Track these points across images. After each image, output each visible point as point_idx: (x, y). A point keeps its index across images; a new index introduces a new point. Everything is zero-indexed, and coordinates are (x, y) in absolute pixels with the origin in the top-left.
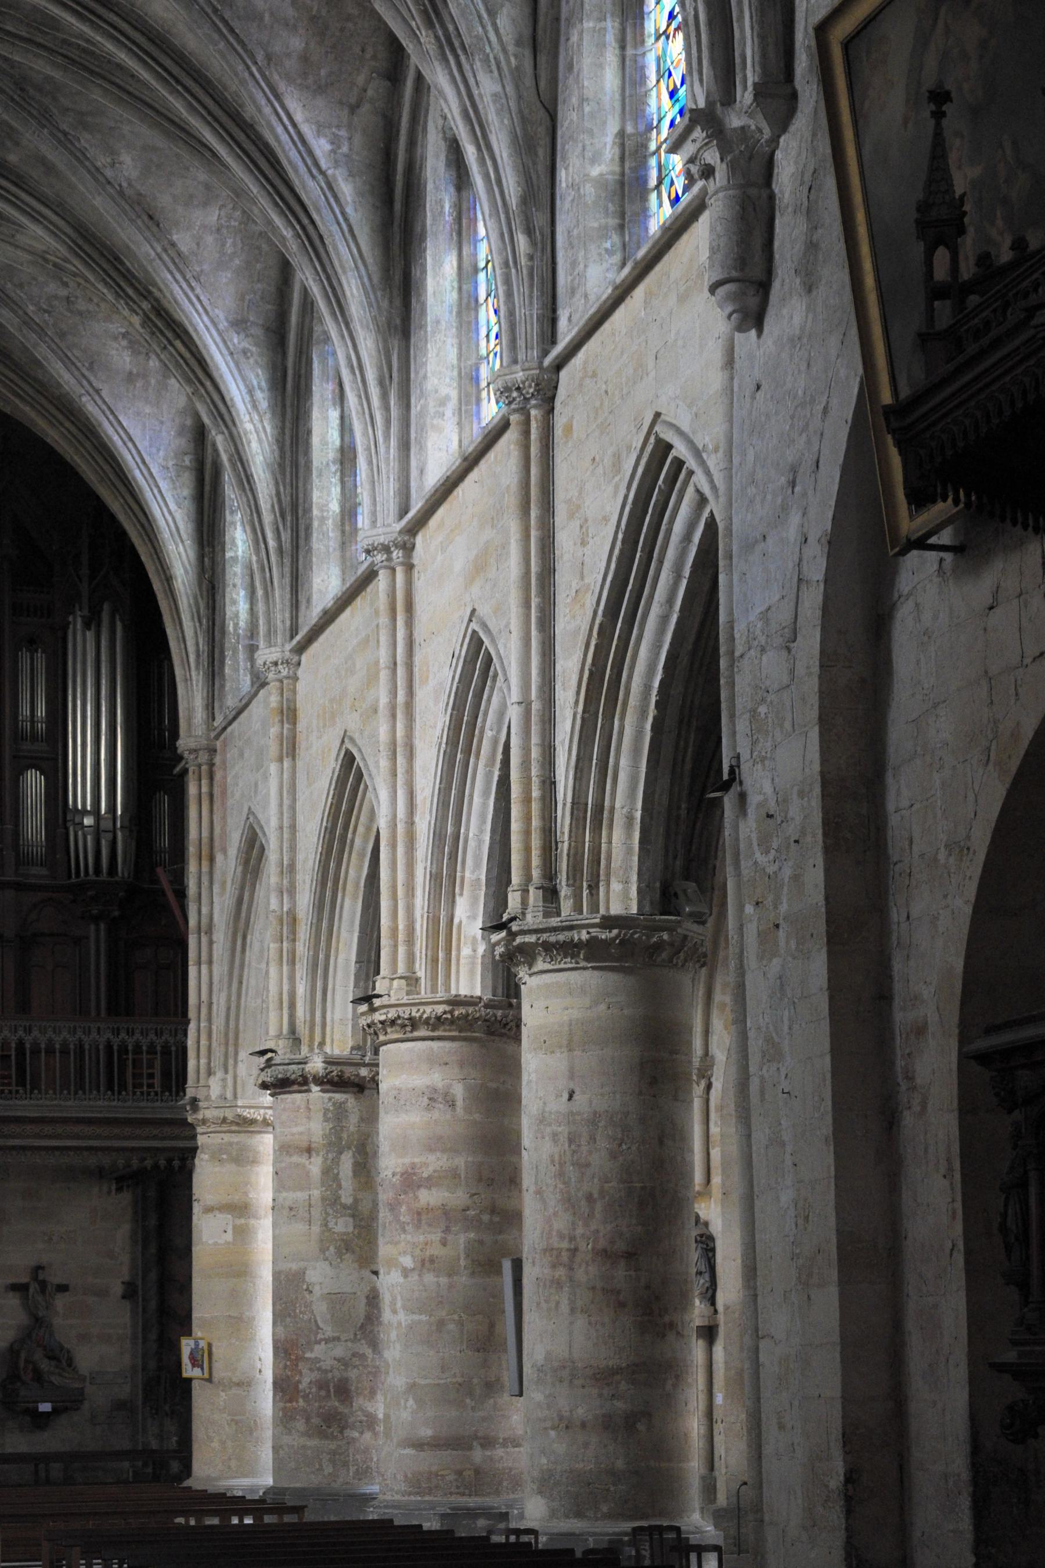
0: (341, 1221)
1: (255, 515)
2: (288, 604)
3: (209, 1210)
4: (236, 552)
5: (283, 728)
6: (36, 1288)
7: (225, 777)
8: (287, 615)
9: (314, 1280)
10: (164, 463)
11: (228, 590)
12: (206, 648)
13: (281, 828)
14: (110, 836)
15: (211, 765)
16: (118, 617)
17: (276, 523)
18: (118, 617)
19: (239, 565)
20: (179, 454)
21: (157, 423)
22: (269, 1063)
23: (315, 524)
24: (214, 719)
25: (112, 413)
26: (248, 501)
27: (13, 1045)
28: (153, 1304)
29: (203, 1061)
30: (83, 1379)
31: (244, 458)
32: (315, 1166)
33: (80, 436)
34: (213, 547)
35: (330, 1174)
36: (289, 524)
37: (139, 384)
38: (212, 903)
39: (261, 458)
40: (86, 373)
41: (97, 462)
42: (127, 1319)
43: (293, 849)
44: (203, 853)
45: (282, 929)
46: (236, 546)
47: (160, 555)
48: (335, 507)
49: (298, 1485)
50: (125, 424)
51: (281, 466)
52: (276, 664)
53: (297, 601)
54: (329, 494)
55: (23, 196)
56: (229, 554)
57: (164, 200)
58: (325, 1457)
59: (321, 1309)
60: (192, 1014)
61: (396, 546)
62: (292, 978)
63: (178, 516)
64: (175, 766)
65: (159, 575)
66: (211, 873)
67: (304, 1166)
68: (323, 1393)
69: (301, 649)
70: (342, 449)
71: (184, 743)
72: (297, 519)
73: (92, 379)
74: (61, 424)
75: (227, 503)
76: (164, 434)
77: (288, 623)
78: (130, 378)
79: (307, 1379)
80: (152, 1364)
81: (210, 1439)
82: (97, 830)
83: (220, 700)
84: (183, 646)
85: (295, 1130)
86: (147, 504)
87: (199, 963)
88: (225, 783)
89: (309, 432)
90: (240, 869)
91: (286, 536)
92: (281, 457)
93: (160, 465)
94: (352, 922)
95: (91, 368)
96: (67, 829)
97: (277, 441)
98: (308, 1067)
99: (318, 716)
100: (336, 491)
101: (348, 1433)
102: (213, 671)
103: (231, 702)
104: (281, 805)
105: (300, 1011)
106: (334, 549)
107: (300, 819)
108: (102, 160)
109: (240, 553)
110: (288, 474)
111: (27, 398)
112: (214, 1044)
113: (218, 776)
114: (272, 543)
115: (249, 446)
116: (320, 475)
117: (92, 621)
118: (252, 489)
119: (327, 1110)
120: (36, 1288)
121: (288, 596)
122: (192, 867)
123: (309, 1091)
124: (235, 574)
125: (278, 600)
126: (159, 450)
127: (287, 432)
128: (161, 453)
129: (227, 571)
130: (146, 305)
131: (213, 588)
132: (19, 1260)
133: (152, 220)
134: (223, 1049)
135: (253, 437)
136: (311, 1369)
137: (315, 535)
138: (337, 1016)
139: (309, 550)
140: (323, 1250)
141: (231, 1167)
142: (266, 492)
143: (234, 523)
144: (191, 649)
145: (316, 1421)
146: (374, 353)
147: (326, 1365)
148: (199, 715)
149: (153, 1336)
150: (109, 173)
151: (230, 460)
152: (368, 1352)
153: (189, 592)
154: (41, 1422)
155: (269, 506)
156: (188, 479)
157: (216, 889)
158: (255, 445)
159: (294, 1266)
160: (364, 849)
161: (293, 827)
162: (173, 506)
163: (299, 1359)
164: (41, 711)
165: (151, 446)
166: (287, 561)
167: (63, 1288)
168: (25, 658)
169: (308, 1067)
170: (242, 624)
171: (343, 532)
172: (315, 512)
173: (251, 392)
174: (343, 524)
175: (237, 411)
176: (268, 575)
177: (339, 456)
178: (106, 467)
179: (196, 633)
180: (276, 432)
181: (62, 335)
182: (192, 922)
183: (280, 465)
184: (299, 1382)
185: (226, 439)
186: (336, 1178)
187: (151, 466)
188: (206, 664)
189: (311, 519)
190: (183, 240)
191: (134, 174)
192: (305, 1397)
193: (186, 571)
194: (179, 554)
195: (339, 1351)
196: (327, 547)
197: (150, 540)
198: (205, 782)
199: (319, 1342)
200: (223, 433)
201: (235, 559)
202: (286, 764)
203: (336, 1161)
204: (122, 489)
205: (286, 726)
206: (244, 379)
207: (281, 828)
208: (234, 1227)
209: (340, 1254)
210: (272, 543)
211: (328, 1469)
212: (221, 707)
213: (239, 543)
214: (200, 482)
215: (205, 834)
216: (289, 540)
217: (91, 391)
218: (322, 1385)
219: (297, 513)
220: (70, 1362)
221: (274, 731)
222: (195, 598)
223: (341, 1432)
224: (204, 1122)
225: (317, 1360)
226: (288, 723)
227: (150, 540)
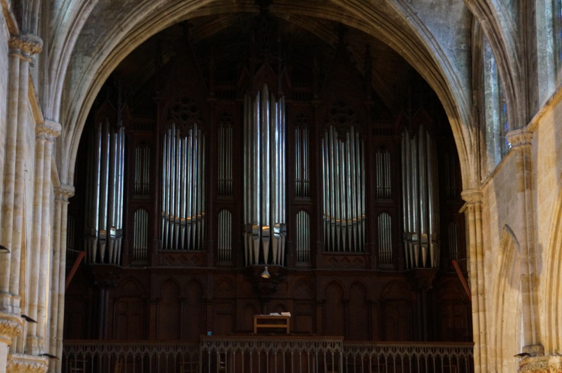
1: (504, 61)
2: (524, 105)
4: (491, 90)
5: (524, 173)
7: (488, 209)
8: (524, 112)
10: (450, 48)
11: (487, 110)
12: (475, 142)
14: (426, 245)
16: (427, 133)
17: (516, 63)
18: (427, 133)
19: (492, 97)
20: (459, 43)
21: (446, 28)
23: (539, 60)
24: (481, 179)
25: (423, 25)
26: (500, 53)
27: (378, 358)
29: (483, 366)
31: (497, 31)
33: (407, 40)
34: (478, 90)
36: (523, 63)
37: (437, 9)
38: (484, 278)
39: (507, 30)
40: (409, 5)
41: (414, 51)
44: (478, 251)
45: (529, 284)
46: (491, 88)
47: (449, 96)
50: (429, 29)
51: (518, 33)
53: (529, 104)
54: (546, 43)
56: (486, 92)
60: (475, 339)
64: (460, 208)
65: (449, 107)
66: (483, 262)
72: (528, 60)
73: (412, 8)
74: (397, 34)
75: (485, 66)
76: (450, 34)
77: (525, 116)
82: (419, 241)
83: (484, 168)
84: (463, 142)
86: (442, 70)
87: (478, 311)
88: (489, 213)
89: (534, 13)
91: (522, 70)
92: (518, 28)
93: (448, 49)
95: (411, 3)
96: (403, 243)
97: (515, 20)
99: (545, 163)
102: (480, 154)
106: (551, 73)
109: (493, 90)
110: (522, 37)
111: (379, 22)
112: (489, 357)
113: (484, 210)
114: (514, 74)
115: (500, 24)
116: (541, 34)
117: (414, 134)
118: (501, 47)
121: (524, 102)
122: (472, 259)
124: (490, 102)
125: (518, 104)
126: (447, 42)
127: (521, 15)
128: (449, 44)
129: (486, 101)
131: (478, 111)
134: (494, 359)
137: (539, 66)
139: (536, 75)
142: (510, 47)
143: (489, 76)
144: (467, 143)
148: (473, 177)
151: (489, 33)
153: (465, 114)
155: (512, 55)
156: (463, 57)
158: (503, 23)
162: (455, 70)
164: (388, 184)
165: (443, 40)
166: (523, 83)
168: (379, 155)
170: (495, 127)
171: (556, 63)
172: (539, 54)
174: (555, 59)
175: (493, 6)
176: (512, 91)
177: (552, 23)
178: (420, 54)
179: (470, 135)
180: (514, 15)
182: (473, 289)
183: (517, 33)
185: (486, 22)
187: (444, 50)
188: (476, 151)
189: (536, 58)
193: (463, 102)
194: (460, 94)
196: (546, 72)
197: (444, 89)
198: (477, 213)
200: (485, 19)
201: (490, 94)
204: (429, 64)
205: (526, 172)
210: (514, 74)
212: (485, 172)
213: (492, 86)
214: (470, 57)
215: (479, 240)
216: (523, 72)
217: (412, 14)
219: (527, 57)
221: (519, 175)
222: (469, 116)
226: (527, 169)
227: (444, 89)
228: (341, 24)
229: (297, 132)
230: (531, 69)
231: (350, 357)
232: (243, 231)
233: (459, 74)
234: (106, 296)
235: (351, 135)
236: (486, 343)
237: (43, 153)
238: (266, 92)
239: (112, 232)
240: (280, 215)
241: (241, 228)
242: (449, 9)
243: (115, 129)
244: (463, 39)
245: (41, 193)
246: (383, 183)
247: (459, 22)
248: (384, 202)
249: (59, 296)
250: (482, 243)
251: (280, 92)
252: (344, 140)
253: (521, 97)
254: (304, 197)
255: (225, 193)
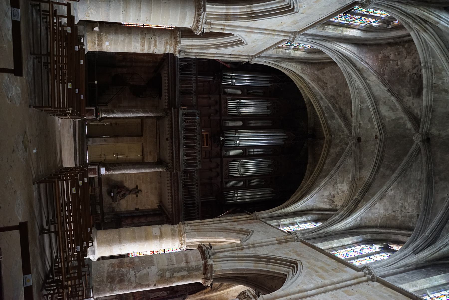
0: (169, 274)
3: (160, 229)
6: (137, 191)
9: (152, 268)
13: (262, 243)
15: (253, 219)
22: (208, 248)
28: (135, 214)
30: (119, 201)
32: (183, 265)
35: (181, 269)
42: (132, 209)
43: (259, 246)
48: (334, 246)
49: (93, 271)
51: (336, 232)
52: (297, 236)
55: (375, 172)
57: (385, 200)
58: (101, 278)
59: (144, 271)
60: (203, 221)
61: (372, 276)
62: (228, 251)
63: (299, 207)
67: (182, 262)
68: (120, 275)
69: (301, 241)
70: (345, 245)
71: (257, 213)
78: (323, 196)
79: (124, 270)
80: (122, 215)
81: (106, 235)
85: (192, 257)
90: (238, 229)
91: (323, 235)
94: (247, 266)
98: (209, 260)
100: (337, 245)
101: (109, 284)
103: (268, 222)
104: (267, 242)
105: (221, 255)
107: (265, 247)
108: (392, 187)
113: (251, 221)
116: (340, 241)
119: (198, 266)
120: (137, 191)
123: (202, 260)
130: (360, 198)
132: (143, 187)
133: (381, 198)
135: (341, 225)
136: (127, 271)
138: (222, 265)
140: (161, 270)
141: (171, 234)
145: (112, 274)
146: (411, 262)
147: (129, 276)
148: (263, 216)
149: (128, 215)
150: (390, 189)
151: (334, 220)
152: (133, 286)
154: (109, 194)
157: (229, 223)
159: (155, 262)
160: (268, 268)
161: (263, 246)
163: (130, 267)
166: (318, 236)
167: (137, 196)
169: (209, 260)
173: (350, 223)
181: (330, 182)
182: (221, 219)
184: (123, 268)
186: (180, 271)
190: (377, 205)
191: (389, 194)
192: (119, 270)
195: (133, 279)
199: (135, 272)
201: (294, 220)
202: (277, 242)
203: (185, 270)
206: (352, 221)
207: (262, 243)
208: (157, 236)
209: (160, 275)
210: (321, 231)
211: (98, 280)
215: (240, 219)
218: (123, 275)
220: (122, 199)
223: (109, 282)
224: (180, 226)
225: (130, 273)
228: (307, 164)
229: (271, 150)
230: (324, 238)
231: (193, 172)
232: (236, 130)
233: (299, 207)
234: (210, 78)
235: (270, 169)
236: (202, 225)
237: (286, 34)
238: (286, 137)
239: (234, 80)
240: (243, 144)
241: (237, 129)
242: (321, 202)
243: (270, 82)
244: (310, 208)
245: (270, 33)
246: (253, 182)
247: (316, 206)
248: (246, 182)
249: (214, 56)
250: (239, 221)
251: (286, 142)
252: (268, 167)
253: (313, 235)
254: (248, 154)
255: (248, 123)
